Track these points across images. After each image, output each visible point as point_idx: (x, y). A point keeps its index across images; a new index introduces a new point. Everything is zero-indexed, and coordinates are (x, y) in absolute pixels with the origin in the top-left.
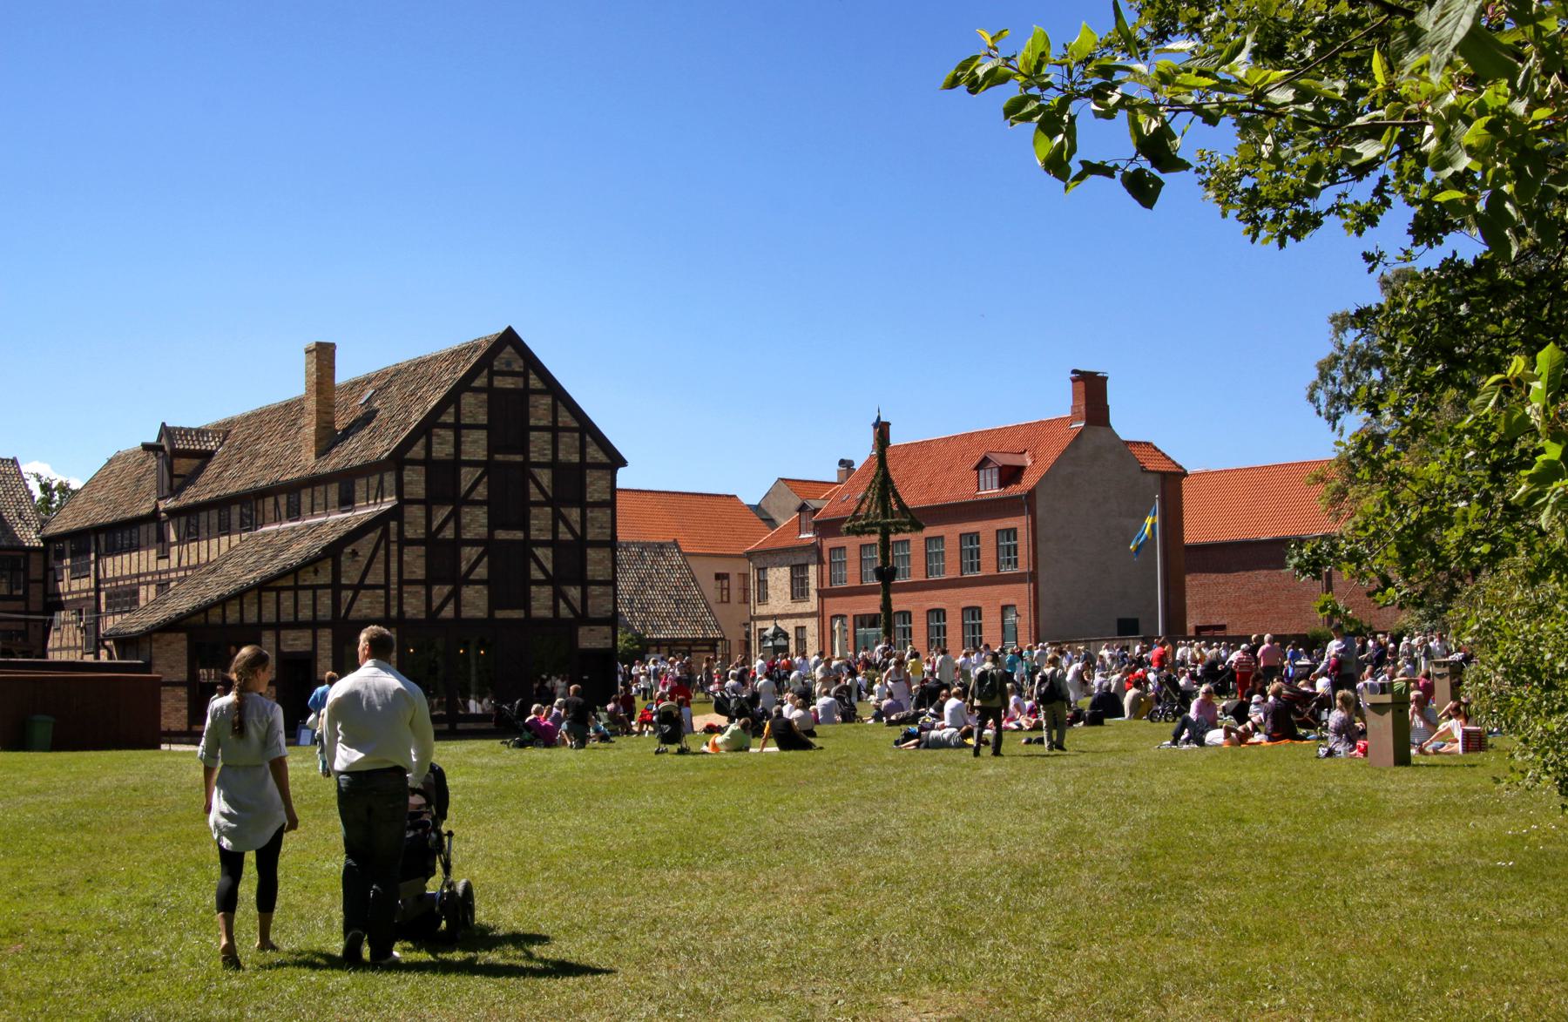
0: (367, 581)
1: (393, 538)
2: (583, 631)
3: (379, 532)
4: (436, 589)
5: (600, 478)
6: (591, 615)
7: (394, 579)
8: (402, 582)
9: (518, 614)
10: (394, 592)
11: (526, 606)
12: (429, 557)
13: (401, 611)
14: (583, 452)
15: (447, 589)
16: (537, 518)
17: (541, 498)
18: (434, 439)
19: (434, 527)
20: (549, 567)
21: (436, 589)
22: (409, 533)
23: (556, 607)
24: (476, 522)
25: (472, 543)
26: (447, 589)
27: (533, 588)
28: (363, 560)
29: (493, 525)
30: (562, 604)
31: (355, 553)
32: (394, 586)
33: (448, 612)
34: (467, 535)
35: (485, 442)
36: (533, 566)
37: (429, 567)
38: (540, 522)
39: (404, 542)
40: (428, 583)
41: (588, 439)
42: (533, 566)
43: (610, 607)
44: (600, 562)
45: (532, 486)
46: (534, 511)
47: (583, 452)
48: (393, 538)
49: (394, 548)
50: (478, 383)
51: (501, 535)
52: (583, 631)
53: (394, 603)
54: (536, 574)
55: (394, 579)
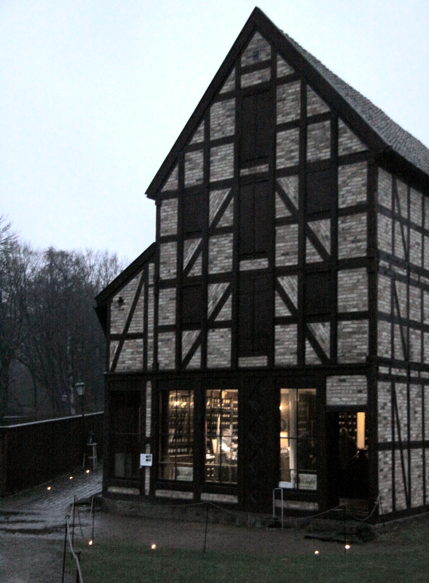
0: (131, 331)
1: (151, 281)
2: (331, 383)
3: (140, 275)
4: (186, 334)
5: (354, 175)
6: (342, 361)
7: (151, 326)
8: (158, 329)
9: (260, 361)
10: (150, 341)
11: (271, 353)
12: (180, 300)
13: (156, 363)
14: (334, 146)
15: (195, 334)
16: (283, 240)
17: (287, 213)
18: (187, 165)
19: (185, 265)
20: (294, 299)
21: (186, 334)
22: (164, 276)
23: (302, 253)
24: (222, 252)
25: (218, 278)
26: (195, 334)
27: (278, 329)
28: (127, 308)
29: (239, 255)
30: (309, 348)
31: (121, 301)
32: (151, 334)
33: (195, 362)
34: (214, 271)
35: (231, 158)
36: (278, 300)
37: (179, 311)
38: (286, 240)
39: (160, 284)
40: (179, 328)
41: (341, 124)
42: (278, 300)
43: (365, 348)
44: (353, 288)
45: (278, 199)
46: (280, 231)
47: (334, 146)
48: (151, 281)
49: (151, 291)
50: (225, 89)
51: (246, 265)
52: (331, 383)
53: (150, 353)
54: (282, 311)
55: (151, 326)
